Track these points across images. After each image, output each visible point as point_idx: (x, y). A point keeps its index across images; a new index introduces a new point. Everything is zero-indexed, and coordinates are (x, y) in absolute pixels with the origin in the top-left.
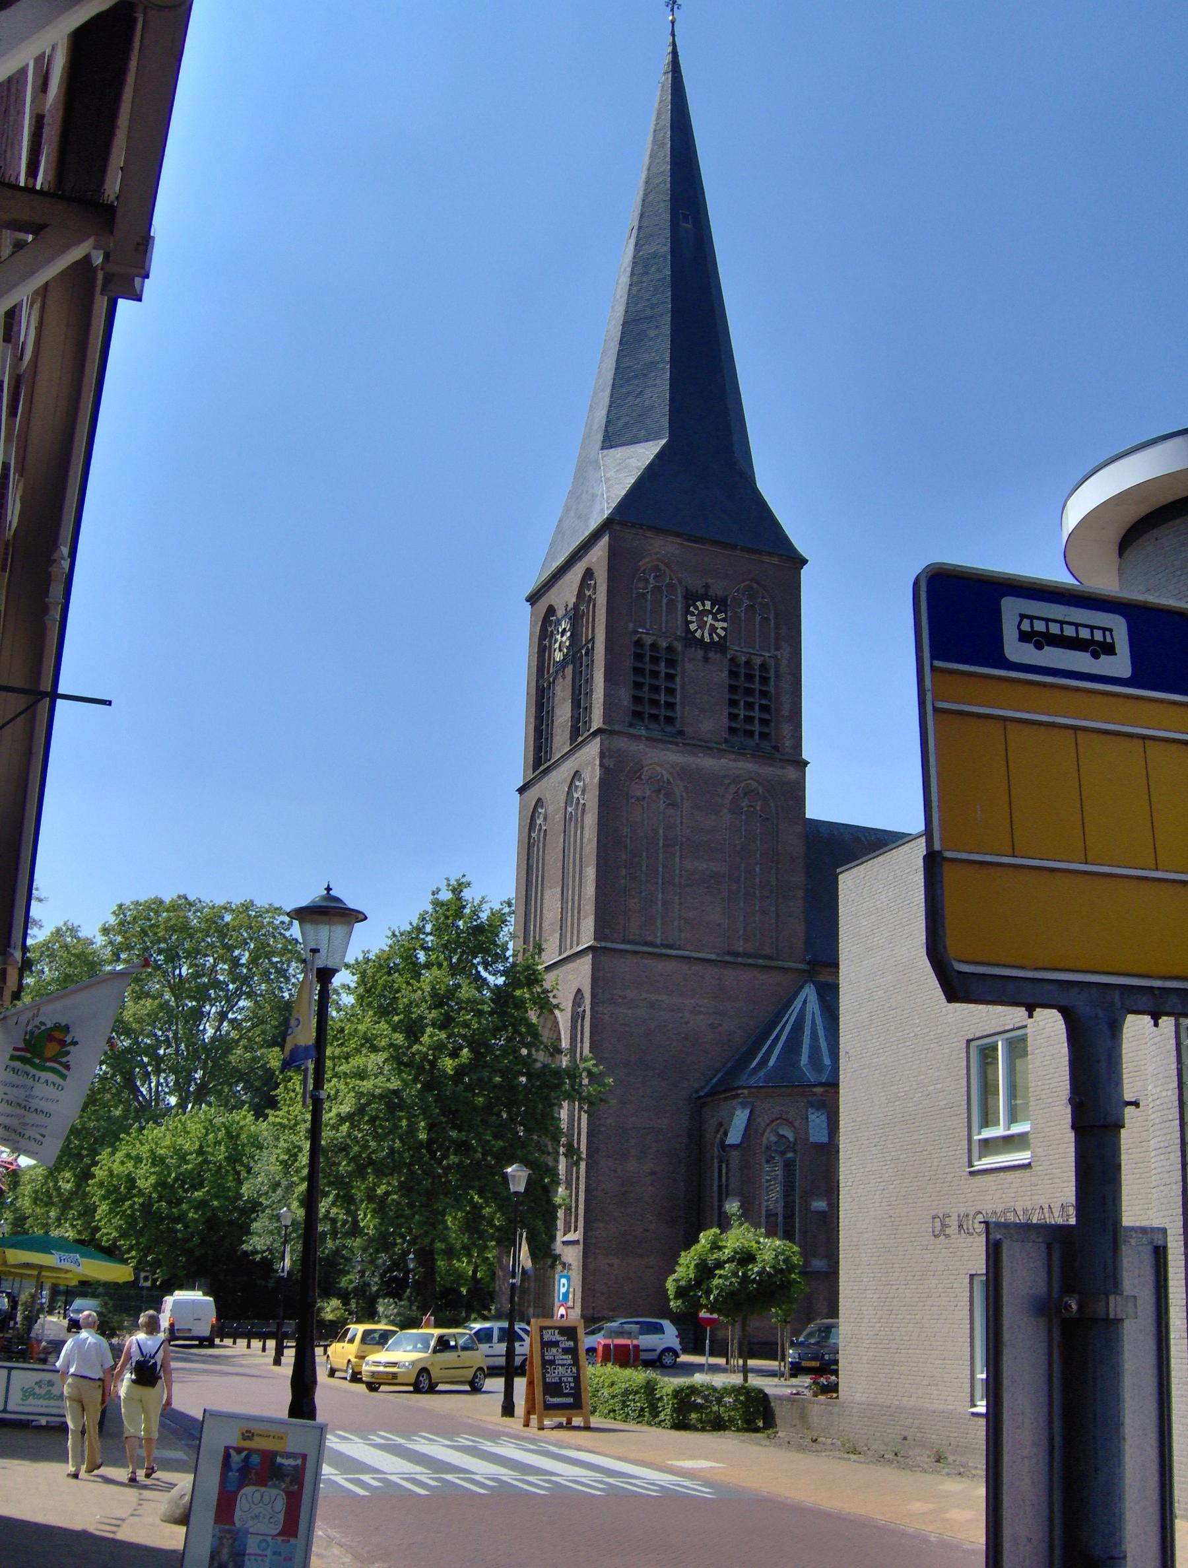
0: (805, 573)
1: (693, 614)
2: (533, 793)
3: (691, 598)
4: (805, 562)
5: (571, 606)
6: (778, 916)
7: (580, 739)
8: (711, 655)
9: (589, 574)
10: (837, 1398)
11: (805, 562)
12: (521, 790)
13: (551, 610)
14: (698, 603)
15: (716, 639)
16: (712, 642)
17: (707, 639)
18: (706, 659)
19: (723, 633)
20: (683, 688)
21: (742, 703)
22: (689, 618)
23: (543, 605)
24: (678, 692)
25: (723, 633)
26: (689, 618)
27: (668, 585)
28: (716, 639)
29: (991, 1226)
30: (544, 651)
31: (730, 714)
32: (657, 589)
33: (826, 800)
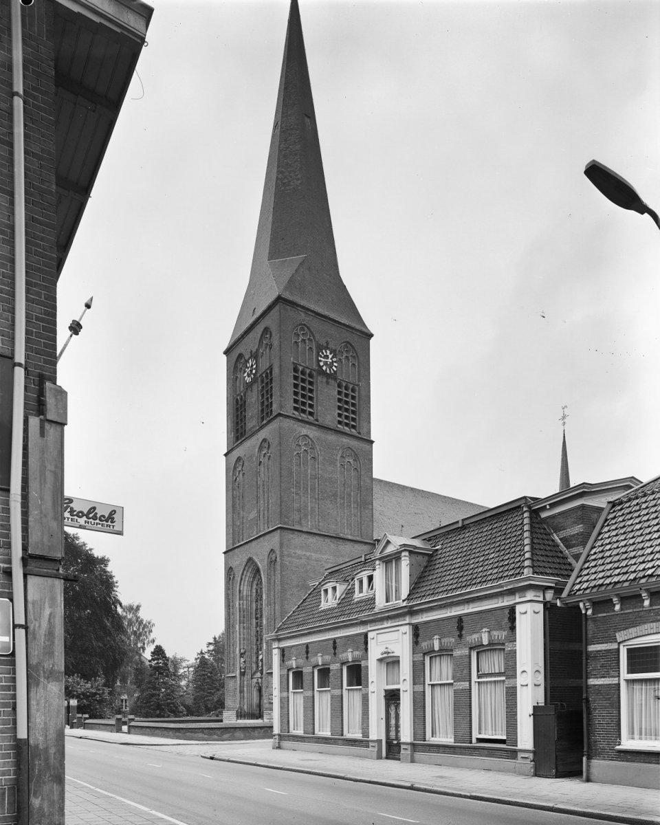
0: (372, 341)
1: (321, 357)
2: (236, 454)
3: (320, 348)
4: (372, 335)
5: (254, 350)
6: (361, 517)
7: (265, 422)
8: (330, 380)
9: (266, 330)
10: (379, 757)
11: (372, 335)
12: (226, 455)
13: (241, 356)
14: (324, 351)
15: (332, 372)
16: (331, 374)
17: (328, 371)
18: (328, 383)
19: (335, 369)
20: (317, 396)
21: (300, 386)
22: (320, 358)
23: (235, 355)
24: (357, 398)
25: (335, 369)
26: (320, 358)
27: (309, 339)
28: (332, 372)
29: (287, 295)
30: (236, 380)
31: (338, 391)
32: (303, 341)
33: (15, 89)
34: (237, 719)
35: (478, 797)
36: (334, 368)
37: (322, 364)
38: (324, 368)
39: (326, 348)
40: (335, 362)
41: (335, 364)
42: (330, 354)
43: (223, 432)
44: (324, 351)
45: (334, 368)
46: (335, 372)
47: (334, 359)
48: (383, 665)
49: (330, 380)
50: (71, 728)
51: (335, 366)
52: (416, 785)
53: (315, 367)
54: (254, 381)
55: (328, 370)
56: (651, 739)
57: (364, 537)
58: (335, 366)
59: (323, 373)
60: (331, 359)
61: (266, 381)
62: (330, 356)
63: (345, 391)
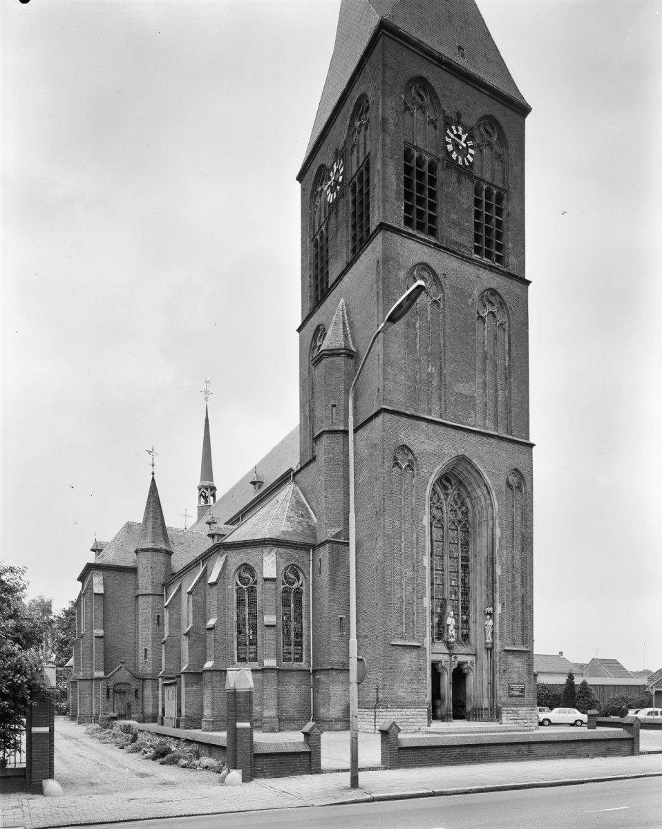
12: (299, 330)
14: (453, 127)
15: (467, 164)
18: (459, 181)
19: (471, 159)
22: (447, 139)
25: (471, 159)
26: (447, 139)
28: (467, 164)
34: (434, 715)
35: (489, 788)
36: (469, 156)
37: (450, 148)
38: (454, 155)
39: (458, 123)
40: (472, 147)
41: (471, 151)
42: (464, 133)
43: (352, 273)
44: (453, 127)
45: (469, 156)
46: (471, 164)
47: (470, 143)
48: (232, 685)
49: (463, 179)
50: (247, 778)
51: (471, 155)
52: (436, 790)
53: (440, 155)
54: (341, 195)
55: (460, 159)
56: (476, 721)
57: (515, 432)
58: (471, 155)
59: (451, 164)
60: (465, 142)
61: (359, 191)
62: (464, 137)
63: (428, 212)
